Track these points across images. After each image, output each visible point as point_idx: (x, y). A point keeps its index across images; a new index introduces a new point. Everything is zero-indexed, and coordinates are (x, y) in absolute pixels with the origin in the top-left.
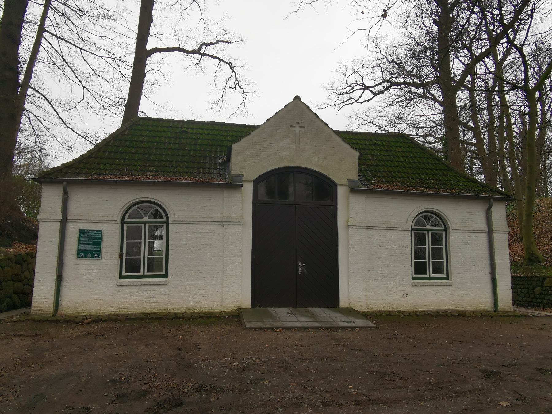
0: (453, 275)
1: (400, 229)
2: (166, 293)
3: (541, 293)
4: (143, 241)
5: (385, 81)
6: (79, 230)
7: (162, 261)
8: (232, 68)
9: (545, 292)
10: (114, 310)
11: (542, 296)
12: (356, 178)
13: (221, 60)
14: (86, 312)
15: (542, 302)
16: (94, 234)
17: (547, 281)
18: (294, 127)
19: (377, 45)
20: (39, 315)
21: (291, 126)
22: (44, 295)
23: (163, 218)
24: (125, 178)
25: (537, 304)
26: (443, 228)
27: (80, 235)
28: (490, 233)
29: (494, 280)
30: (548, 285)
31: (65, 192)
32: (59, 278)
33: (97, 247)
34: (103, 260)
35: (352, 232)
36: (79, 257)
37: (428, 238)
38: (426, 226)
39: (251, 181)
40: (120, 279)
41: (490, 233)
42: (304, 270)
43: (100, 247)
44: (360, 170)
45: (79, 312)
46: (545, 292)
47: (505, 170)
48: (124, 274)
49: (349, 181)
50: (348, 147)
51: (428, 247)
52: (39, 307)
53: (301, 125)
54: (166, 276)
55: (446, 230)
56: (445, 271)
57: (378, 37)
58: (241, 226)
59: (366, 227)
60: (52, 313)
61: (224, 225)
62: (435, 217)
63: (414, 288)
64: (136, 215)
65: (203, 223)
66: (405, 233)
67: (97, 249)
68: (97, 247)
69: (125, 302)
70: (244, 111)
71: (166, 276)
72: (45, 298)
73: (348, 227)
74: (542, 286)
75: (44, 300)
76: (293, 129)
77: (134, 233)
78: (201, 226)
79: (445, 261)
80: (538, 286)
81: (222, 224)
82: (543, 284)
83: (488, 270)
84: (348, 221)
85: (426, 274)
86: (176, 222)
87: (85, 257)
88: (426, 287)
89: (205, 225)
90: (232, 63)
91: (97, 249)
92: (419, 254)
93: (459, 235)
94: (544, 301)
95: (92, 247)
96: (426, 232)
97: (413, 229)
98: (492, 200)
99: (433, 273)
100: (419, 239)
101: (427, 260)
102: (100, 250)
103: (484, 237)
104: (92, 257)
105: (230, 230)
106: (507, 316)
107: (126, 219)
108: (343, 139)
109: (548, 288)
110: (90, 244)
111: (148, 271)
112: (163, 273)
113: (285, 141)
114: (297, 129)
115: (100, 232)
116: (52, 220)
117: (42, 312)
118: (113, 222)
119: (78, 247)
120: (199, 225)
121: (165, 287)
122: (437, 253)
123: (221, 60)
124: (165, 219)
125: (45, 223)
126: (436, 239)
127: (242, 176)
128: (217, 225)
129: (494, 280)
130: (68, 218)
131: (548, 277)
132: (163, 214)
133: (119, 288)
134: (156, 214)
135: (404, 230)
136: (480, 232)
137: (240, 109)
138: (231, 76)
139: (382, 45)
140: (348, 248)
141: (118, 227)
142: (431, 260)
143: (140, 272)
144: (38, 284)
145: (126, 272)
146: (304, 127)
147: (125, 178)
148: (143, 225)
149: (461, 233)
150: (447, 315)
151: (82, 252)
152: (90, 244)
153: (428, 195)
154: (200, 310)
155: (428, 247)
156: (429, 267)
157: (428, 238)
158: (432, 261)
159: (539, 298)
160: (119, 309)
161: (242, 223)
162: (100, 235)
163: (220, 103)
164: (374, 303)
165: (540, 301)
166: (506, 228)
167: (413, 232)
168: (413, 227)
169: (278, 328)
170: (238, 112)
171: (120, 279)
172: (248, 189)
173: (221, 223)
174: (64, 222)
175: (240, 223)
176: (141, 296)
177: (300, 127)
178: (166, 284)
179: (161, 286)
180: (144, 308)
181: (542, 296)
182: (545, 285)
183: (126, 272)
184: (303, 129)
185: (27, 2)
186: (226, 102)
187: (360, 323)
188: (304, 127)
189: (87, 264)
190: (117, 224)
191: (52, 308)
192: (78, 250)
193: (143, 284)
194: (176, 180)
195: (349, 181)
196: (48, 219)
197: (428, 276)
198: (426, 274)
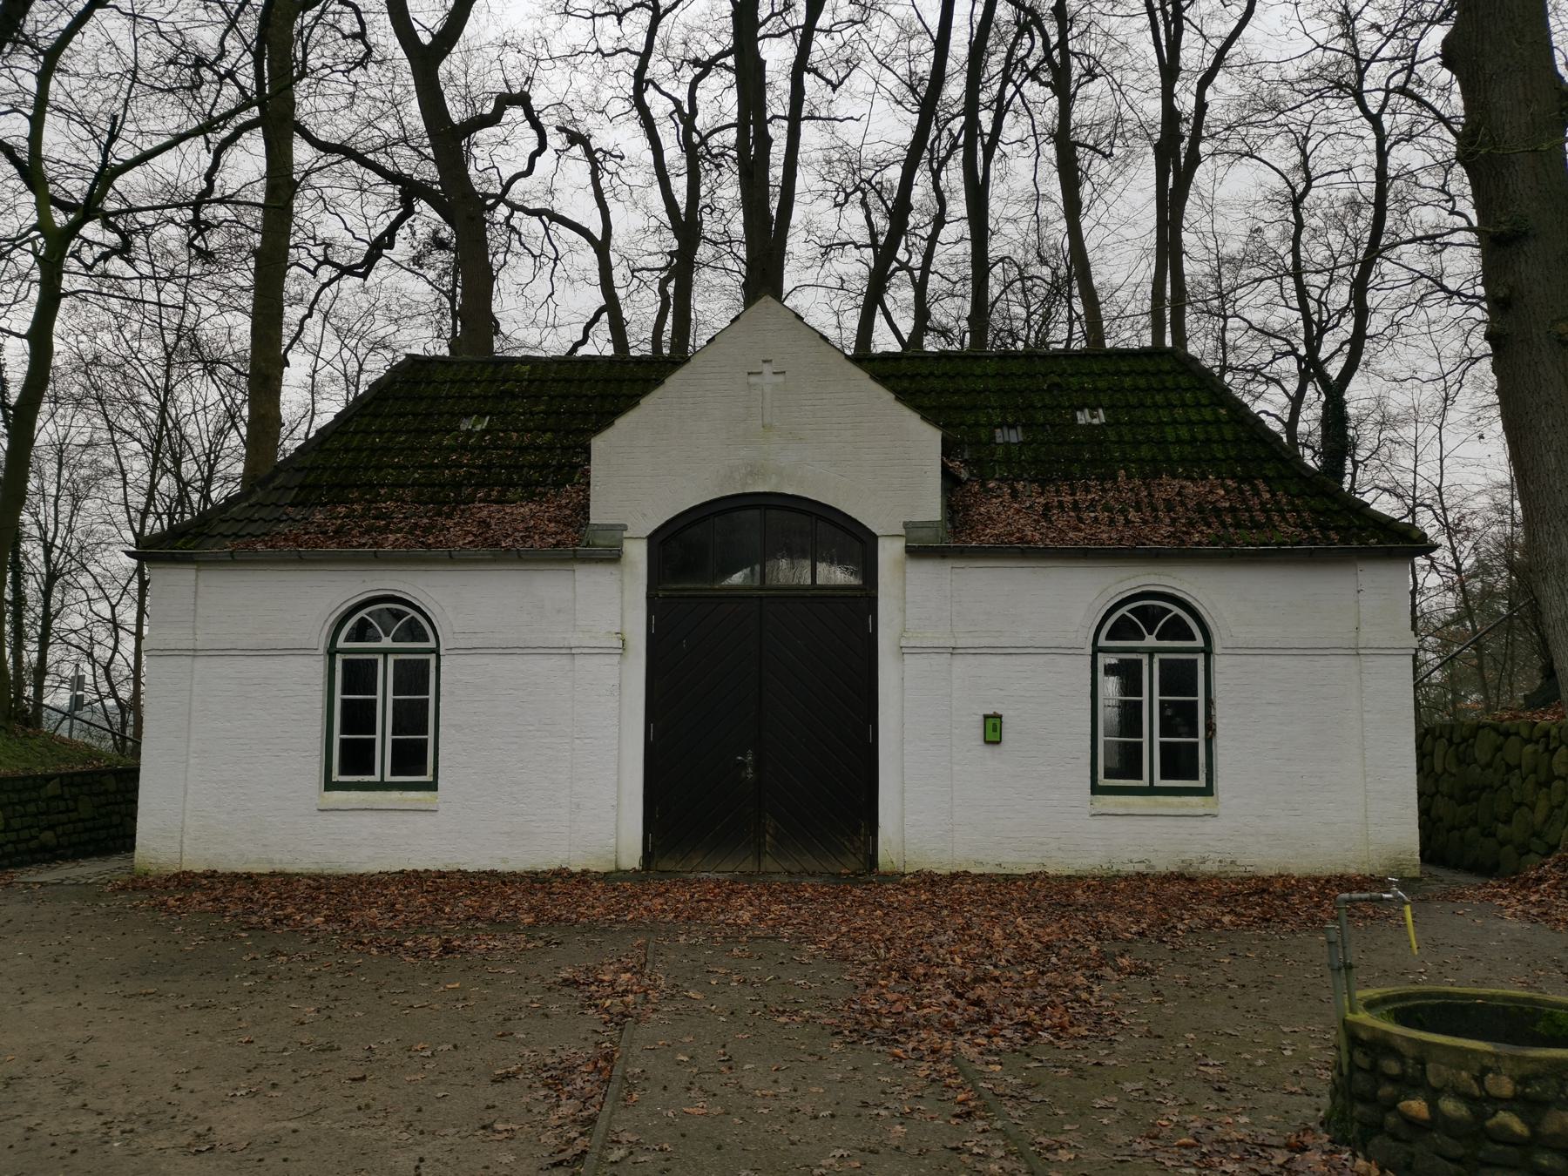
23: (1193, 638)
26: (432, 644)
37: (1151, 678)
38: (1142, 638)
48: (336, 777)
49: (906, 525)
51: (385, 698)
55: (1208, 651)
59: (191, 653)
62: (1176, 610)
64: (362, 631)
65: (1264, 652)
71: (1208, 791)
85: (1140, 777)
86: (1234, 651)
92: (358, 717)
96: (1145, 659)
100: (359, 676)
107: (1102, 642)
118: (1070, 651)
121: (1210, 822)
122: (413, 718)
124: (1199, 642)
127: (624, 528)
134: (1176, 629)
141: (319, 665)
143: (373, 774)
149: (558, 657)
155: (385, 698)
156: (1152, 760)
157: (1151, 678)
158: (1161, 743)
172: (637, 553)
178: (1215, 816)
184: (780, 378)
185: (461, 123)
190: (1080, 658)
195: (906, 525)
198: (1140, 777)
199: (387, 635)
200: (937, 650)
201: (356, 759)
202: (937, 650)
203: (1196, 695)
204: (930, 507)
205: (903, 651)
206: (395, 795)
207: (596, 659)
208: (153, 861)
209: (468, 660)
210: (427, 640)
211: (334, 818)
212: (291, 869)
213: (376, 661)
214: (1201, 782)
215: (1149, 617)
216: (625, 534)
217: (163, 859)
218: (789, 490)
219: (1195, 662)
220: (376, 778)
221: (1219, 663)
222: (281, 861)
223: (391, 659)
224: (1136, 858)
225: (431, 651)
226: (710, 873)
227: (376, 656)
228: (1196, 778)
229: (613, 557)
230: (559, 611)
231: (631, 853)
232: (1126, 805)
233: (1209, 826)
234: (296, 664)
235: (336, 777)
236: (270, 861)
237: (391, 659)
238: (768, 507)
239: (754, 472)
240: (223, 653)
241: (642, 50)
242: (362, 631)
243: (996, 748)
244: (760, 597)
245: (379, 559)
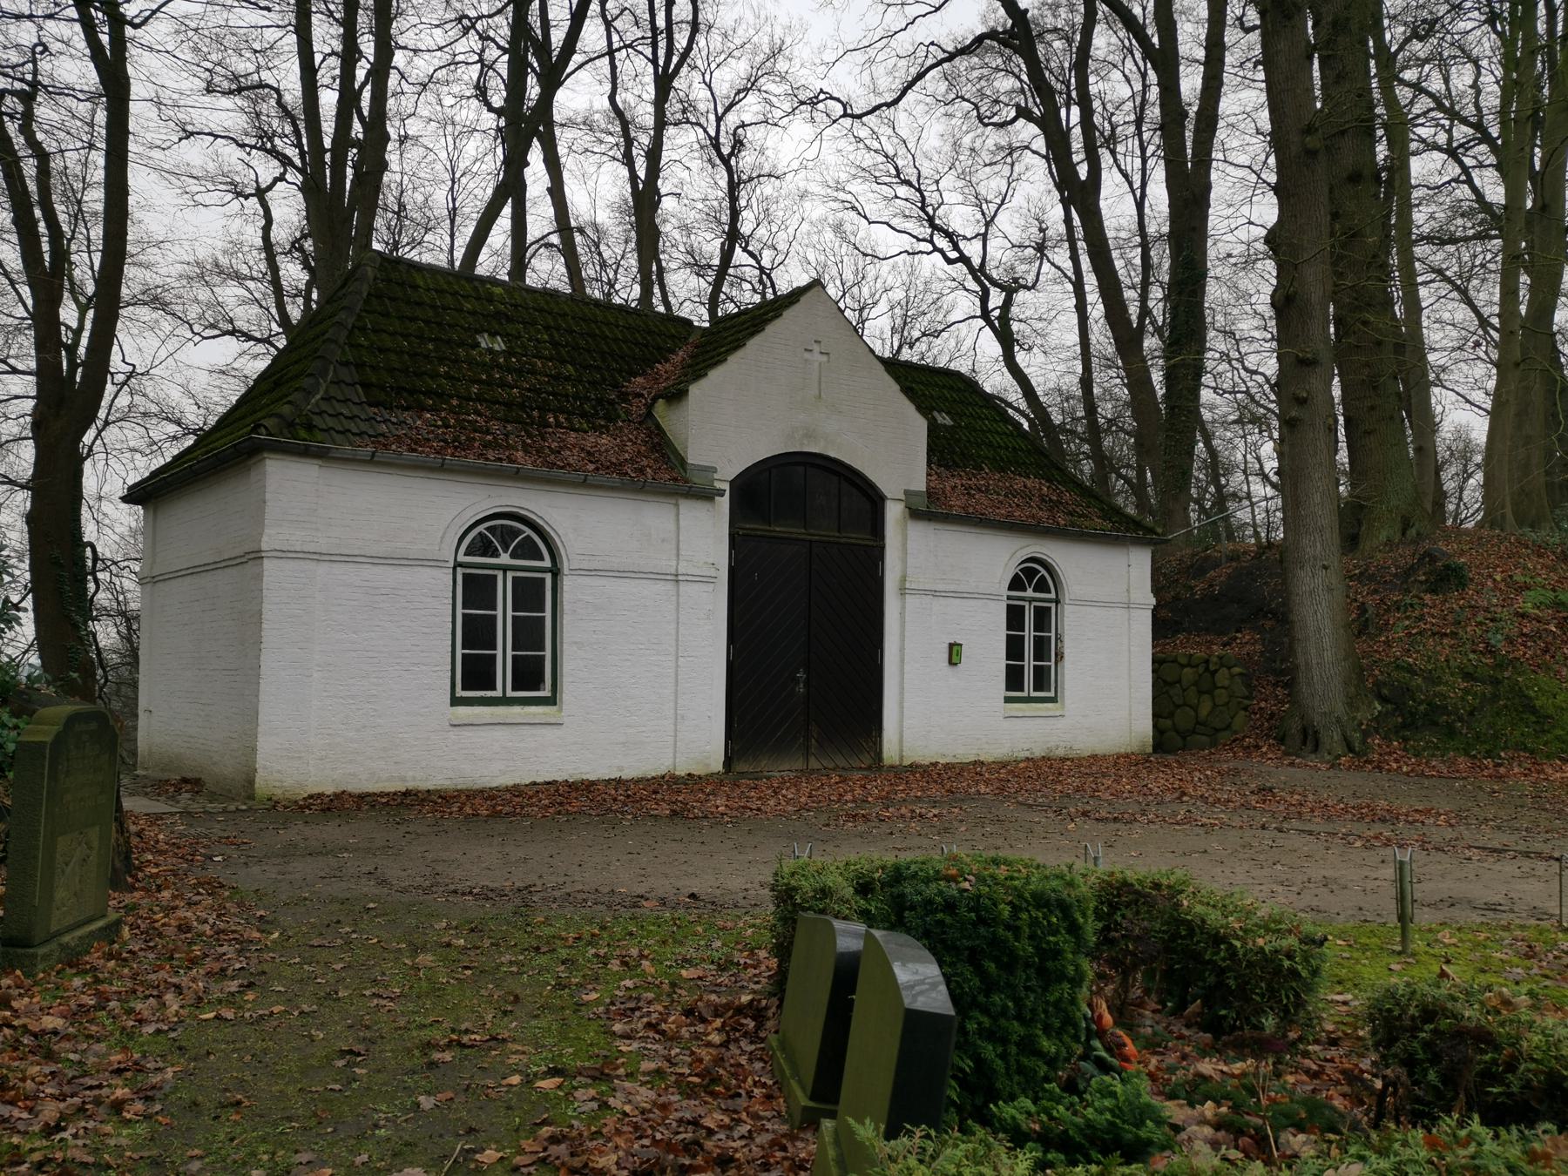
0: (1067, 693)
23: (542, 559)
26: (1053, 596)
40: (452, 705)
47: (1443, 506)
48: (546, 693)
49: (907, 492)
51: (504, 613)
55: (556, 572)
62: (529, 532)
71: (551, 701)
76: (807, 355)
79: (548, 653)
84: (904, 579)
92: (477, 632)
97: (457, 565)
100: (477, 590)
108: (908, 391)
122: (529, 634)
124: (547, 563)
126: (529, 594)
127: (715, 470)
134: (1042, 586)
135: (436, 563)
142: (1032, 663)
149: (662, 583)
155: (504, 613)
167: (460, 571)
168: (461, 558)
171: (452, 705)
184: (824, 358)
195: (907, 492)
199: (505, 550)
201: (1014, 679)
203: (543, 611)
204: (920, 484)
205: (903, 591)
206: (517, 709)
207: (696, 586)
208: (277, 784)
209: (587, 580)
210: (1050, 592)
211: (467, 733)
212: (592, 777)
213: (495, 577)
214: (546, 693)
215: (507, 535)
216: (716, 476)
217: (288, 783)
218: (832, 454)
219: (543, 580)
220: (498, 693)
221: (567, 583)
222: (414, 779)
223: (510, 575)
224: (1026, 746)
225: (1050, 601)
226: (782, 769)
227: (496, 572)
228: (463, 689)
229: (707, 495)
230: (663, 541)
231: (716, 763)
232: (1020, 710)
233: (1061, 723)
234: (425, 574)
235: (546, 693)
236: (403, 779)
237: (510, 575)
238: (813, 465)
239: (810, 435)
240: (348, 559)
241: (690, 18)
242: (483, 546)
243: (955, 668)
244: (811, 541)
245: (518, 476)
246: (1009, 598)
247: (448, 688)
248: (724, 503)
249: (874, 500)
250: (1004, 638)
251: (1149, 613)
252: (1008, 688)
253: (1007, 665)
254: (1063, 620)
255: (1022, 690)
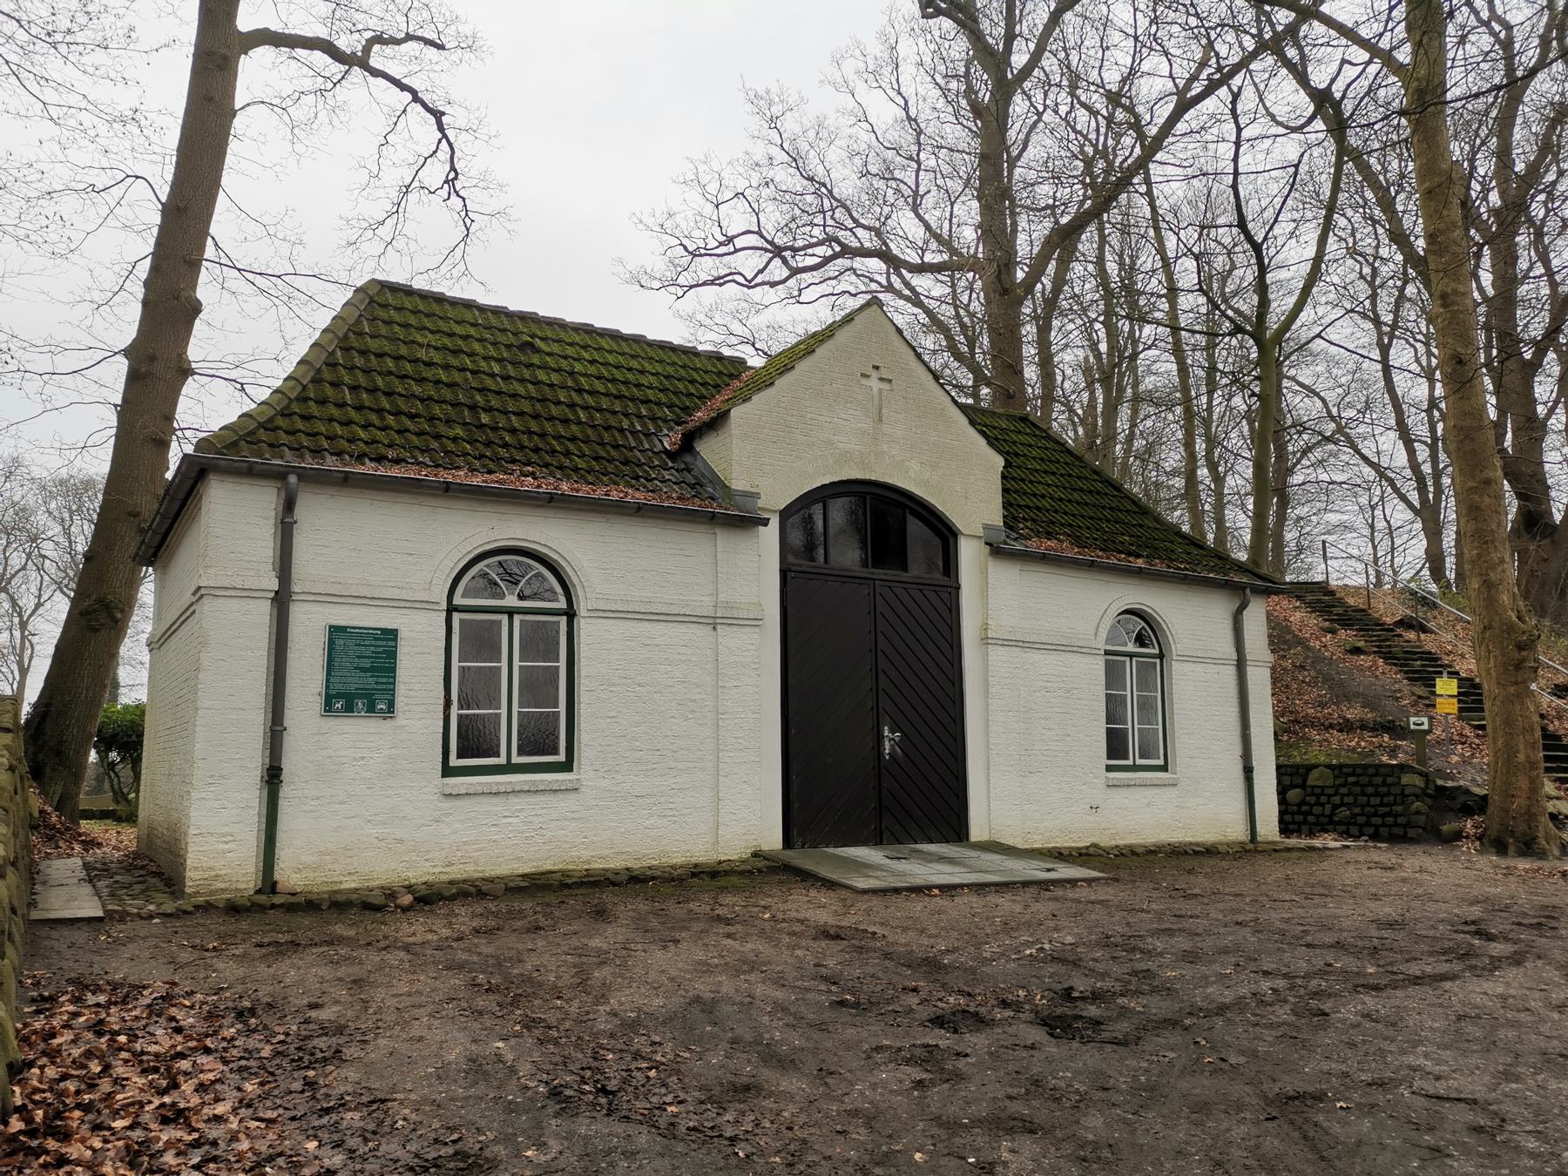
1: (1084, 650)
2: (577, 815)
3: (1303, 802)
4: (504, 664)
5: (830, 240)
6: (331, 627)
7: (557, 727)
8: (441, 128)
9: (1312, 800)
10: (437, 870)
11: (1304, 808)
12: (998, 521)
13: (416, 98)
14: (354, 877)
15: (1305, 822)
16: (376, 639)
17: (1315, 774)
18: (868, 376)
19: (773, 121)
20: (212, 893)
21: (863, 375)
22: (227, 829)
24: (461, 476)
25: (1295, 827)
27: (331, 642)
28: (1241, 665)
29: (1248, 771)
30: (1319, 783)
31: (289, 506)
32: (273, 776)
33: (384, 680)
34: (401, 718)
35: (995, 653)
36: (330, 711)
38: (1126, 645)
39: (775, 511)
41: (1241, 665)
42: (897, 748)
43: (391, 680)
44: (1007, 505)
45: (336, 879)
46: (1312, 800)
48: (454, 761)
50: (982, 442)
52: (211, 868)
53: (885, 374)
54: (567, 766)
55: (570, 614)
56: (1162, 752)
57: (777, 99)
58: (757, 630)
60: (252, 885)
61: (719, 627)
62: (1143, 624)
63: (1109, 791)
66: (1090, 659)
67: (384, 687)
68: (384, 680)
69: (465, 843)
70: (461, 267)
71: (567, 766)
72: (230, 838)
73: (985, 640)
74: (1303, 786)
75: (226, 847)
76: (864, 381)
77: (481, 642)
78: (660, 627)
79: (1160, 727)
80: (1296, 787)
81: (714, 623)
82: (1305, 780)
83: (1237, 750)
84: (985, 627)
86: (599, 614)
87: (349, 708)
88: (1132, 790)
89: (671, 625)
90: (443, 114)
91: (384, 687)
93: (1188, 667)
94: (1311, 819)
95: (369, 681)
98: (1248, 591)
99: (521, 752)
101: (1130, 726)
102: (394, 690)
103: (1230, 672)
104: (371, 709)
105: (731, 639)
106: (1274, 851)
107: (458, 600)
109: (1318, 791)
110: (363, 670)
111: (555, 752)
112: (562, 757)
113: (850, 411)
114: (874, 383)
115: (391, 635)
116: (247, 593)
117: (222, 886)
118: (426, 605)
119: (328, 680)
120: (654, 624)
121: (572, 796)
123: (416, 98)
124: (562, 604)
125: (221, 600)
127: (756, 496)
128: (700, 626)
129: (1248, 771)
130: (296, 588)
131: (1316, 766)
132: (559, 589)
133: (446, 805)
136: (1215, 661)
137: (450, 261)
138: (435, 152)
139: (790, 125)
140: (987, 692)
144: (203, 795)
145: (459, 756)
146: (890, 381)
147: (461, 476)
148: (505, 618)
150: (1186, 852)
151: (339, 696)
152: (363, 670)
153: (1139, 573)
154: (663, 860)
155: (510, 665)
159: (1299, 813)
160: (450, 864)
161: (759, 623)
162: (393, 644)
163: (385, 232)
164: (1037, 829)
165: (1299, 818)
166: (1269, 657)
169: (930, 888)
170: (444, 269)
173: (711, 621)
174: (282, 600)
175: (755, 622)
176: (510, 824)
177: (881, 379)
179: (561, 796)
180: (518, 859)
181: (1304, 808)
182: (1309, 782)
183: (459, 756)
184: (885, 386)
186: (404, 231)
187: (1065, 871)
188: (890, 381)
189: (356, 730)
191: (253, 870)
192: (327, 687)
193: (517, 788)
194: (584, 491)
196: (235, 588)
197: (1130, 762)
200: (698, 620)
201: (1116, 745)
202: (698, 620)
221: (584, 627)
231: (773, 839)
237: (517, 619)
246: (1107, 653)
247: (440, 758)
248: (770, 535)
249: (945, 534)
250: (1104, 730)
251: (1268, 672)
252: (1109, 758)
253: (1106, 661)
254: (1172, 718)
255: (1127, 758)
